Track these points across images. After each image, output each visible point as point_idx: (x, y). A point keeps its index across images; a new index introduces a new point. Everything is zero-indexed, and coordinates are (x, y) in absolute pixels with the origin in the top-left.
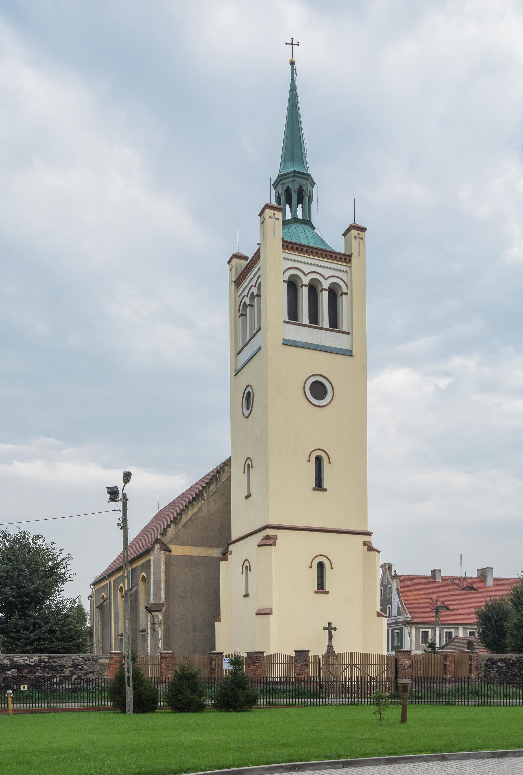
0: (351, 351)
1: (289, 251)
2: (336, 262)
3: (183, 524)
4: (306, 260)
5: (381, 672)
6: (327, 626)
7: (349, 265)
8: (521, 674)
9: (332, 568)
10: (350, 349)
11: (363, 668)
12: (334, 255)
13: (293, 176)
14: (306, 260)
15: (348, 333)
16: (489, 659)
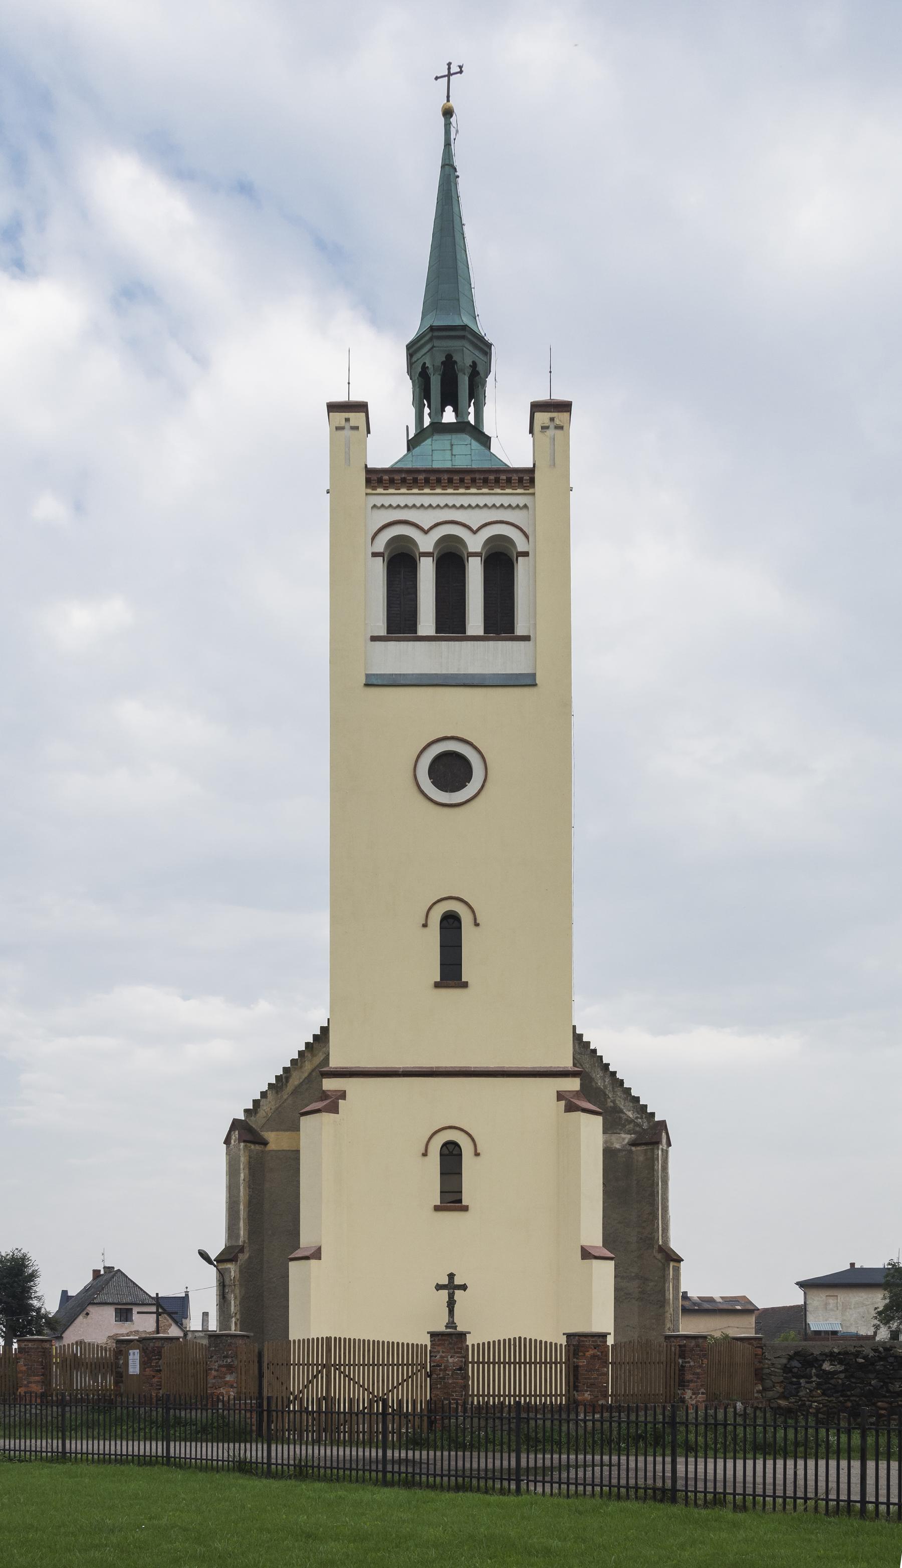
1: (386, 488)
3: (293, 1088)
4: (418, 500)
5: (551, 1386)
6: (457, 1281)
7: (531, 491)
8: (888, 1391)
9: (477, 1154)
10: (530, 671)
11: (355, 1373)
12: (492, 477)
15: (526, 638)
16: (797, 1354)
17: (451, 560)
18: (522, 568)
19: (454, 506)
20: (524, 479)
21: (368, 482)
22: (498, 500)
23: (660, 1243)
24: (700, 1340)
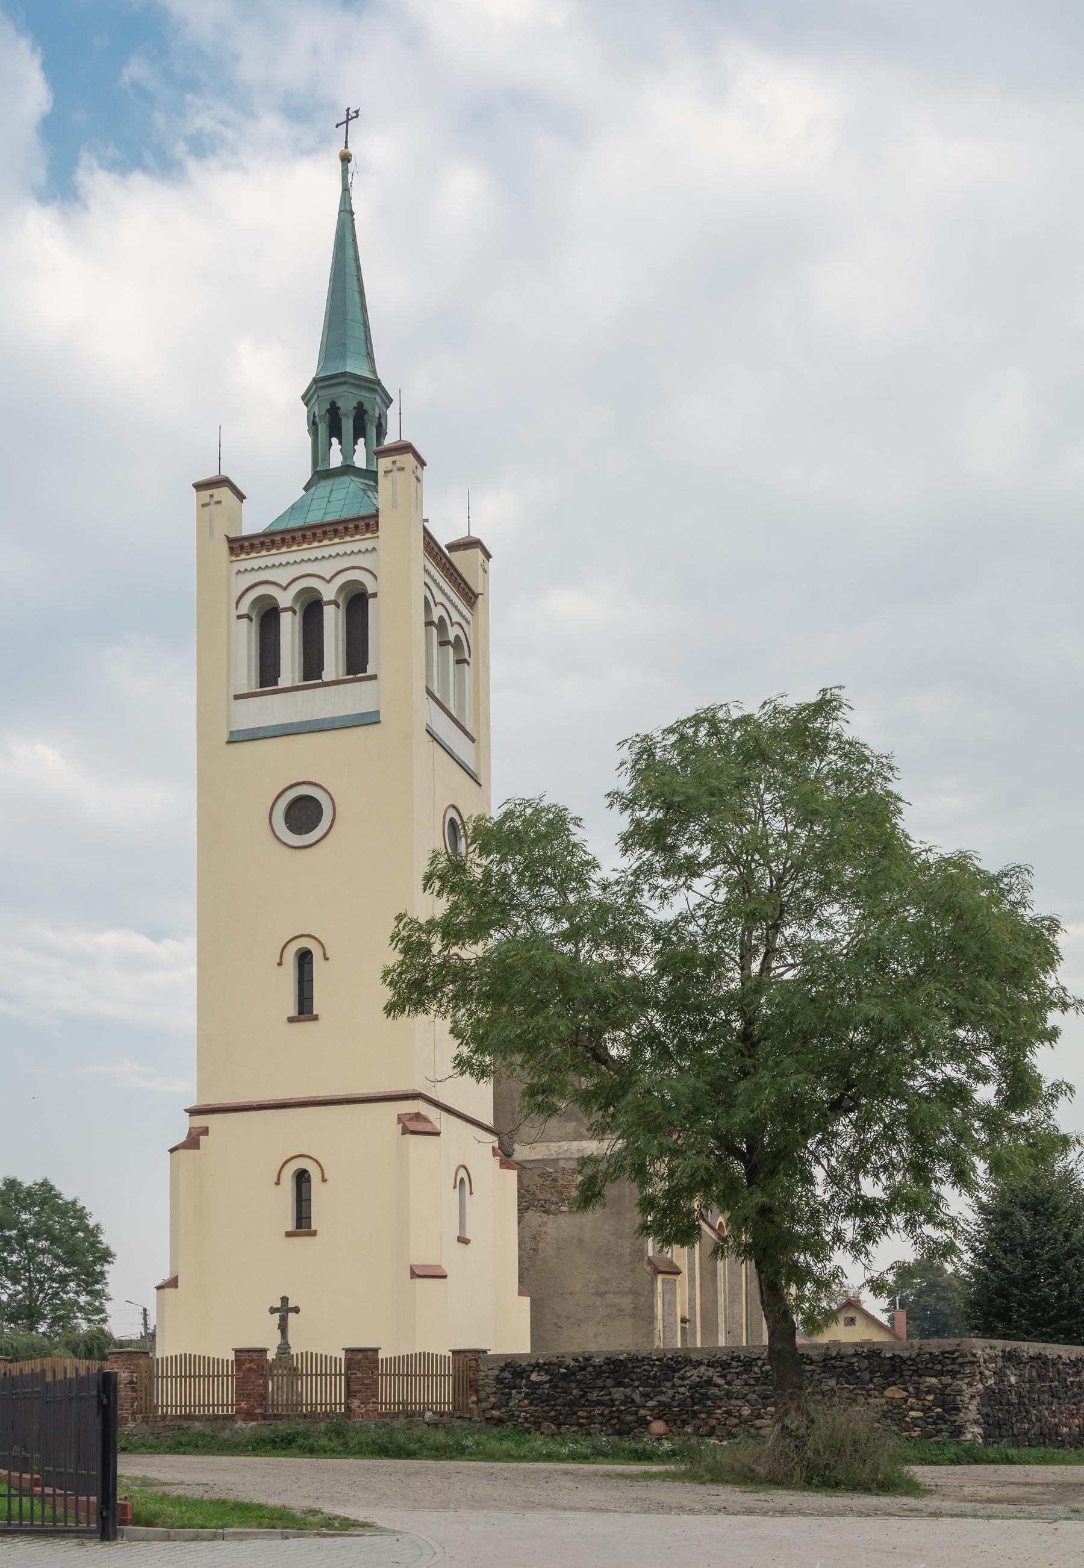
1: (248, 553)
4: (276, 560)
5: (222, 1396)
6: (278, 1305)
8: (587, 1400)
9: (324, 1180)
14: (276, 560)
15: (374, 677)
17: (312, 609)
19: (309, 560)
21: (232, 550)
22: (348, 548)
23: (650, 1254)
24: (370, 1354)
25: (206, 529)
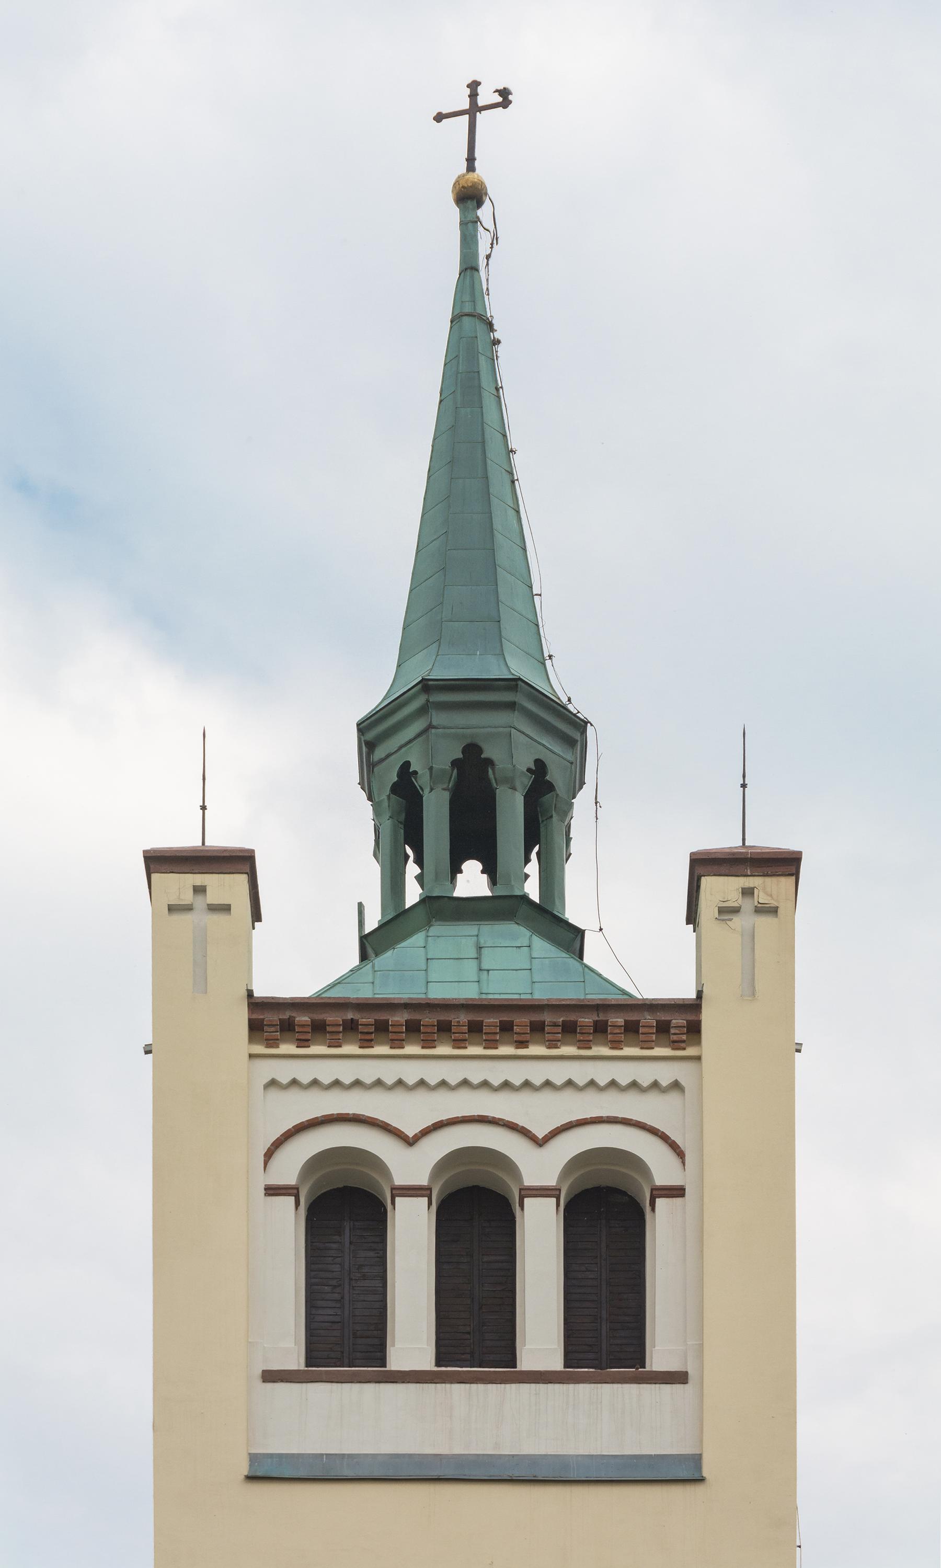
0: (696, 1460)
2: (605, 1051)
4: (389, 1071)
7: (690, 1051)
13: (423, 711)
14: (389, 1071)
15: (678, 1378)
18: (664, 1226)
20: (674, 1024)
21: (256, 1028)
22: (603, 1073)
25: (180, 974)
